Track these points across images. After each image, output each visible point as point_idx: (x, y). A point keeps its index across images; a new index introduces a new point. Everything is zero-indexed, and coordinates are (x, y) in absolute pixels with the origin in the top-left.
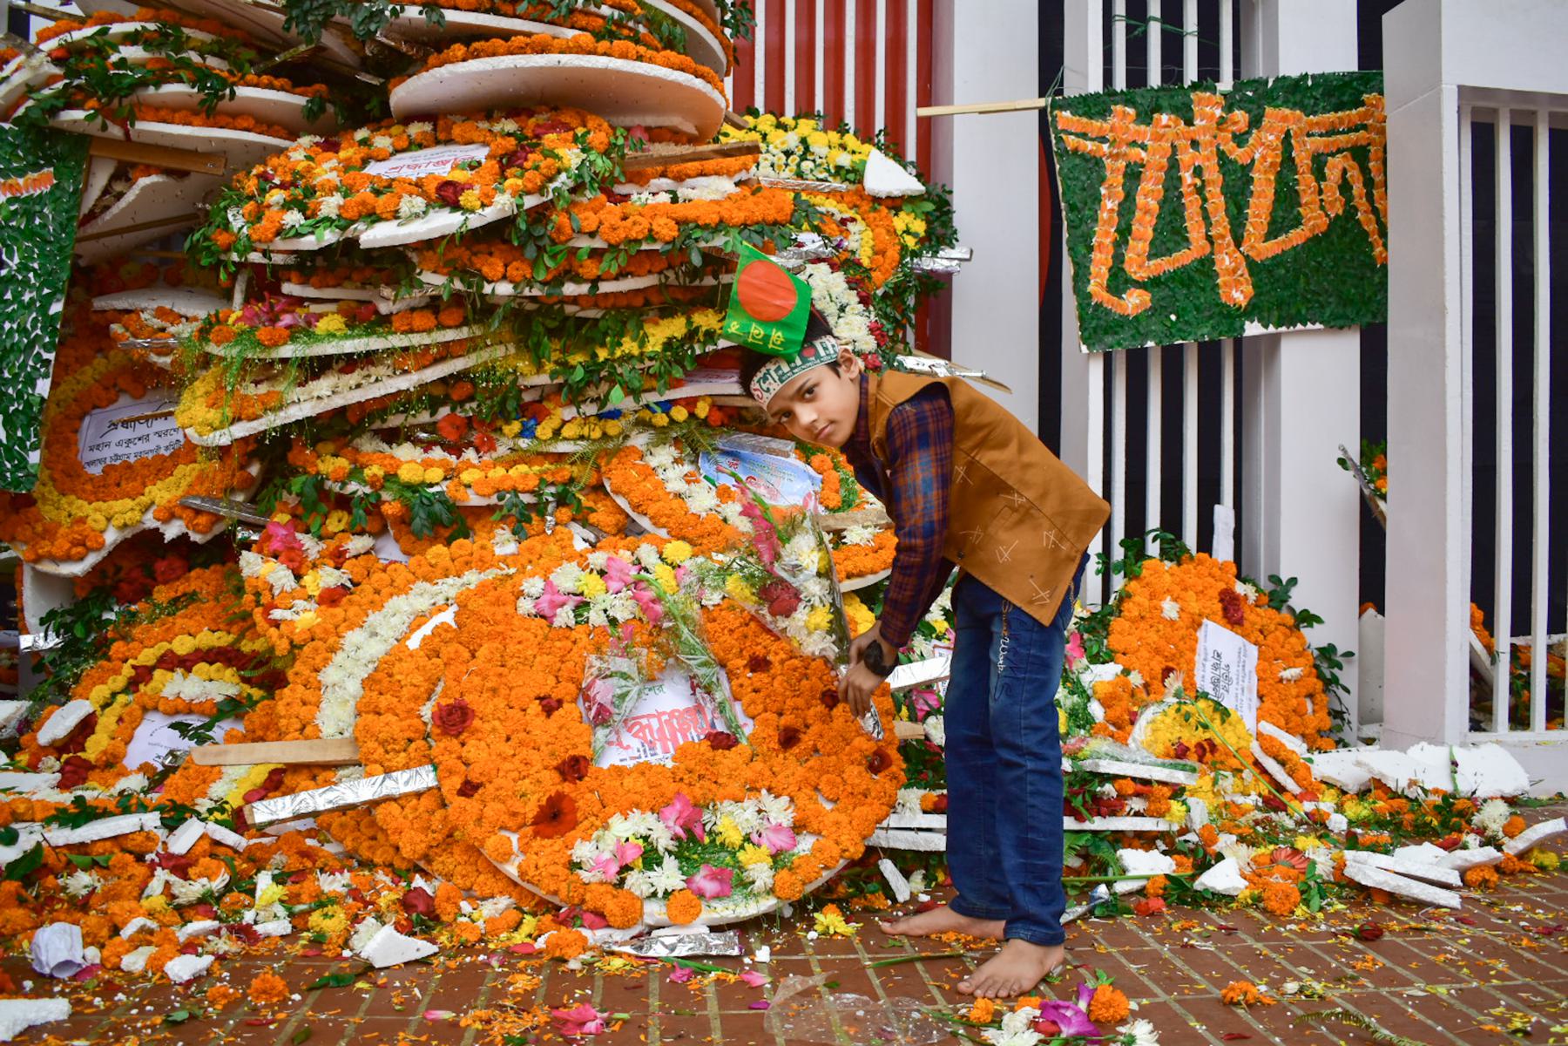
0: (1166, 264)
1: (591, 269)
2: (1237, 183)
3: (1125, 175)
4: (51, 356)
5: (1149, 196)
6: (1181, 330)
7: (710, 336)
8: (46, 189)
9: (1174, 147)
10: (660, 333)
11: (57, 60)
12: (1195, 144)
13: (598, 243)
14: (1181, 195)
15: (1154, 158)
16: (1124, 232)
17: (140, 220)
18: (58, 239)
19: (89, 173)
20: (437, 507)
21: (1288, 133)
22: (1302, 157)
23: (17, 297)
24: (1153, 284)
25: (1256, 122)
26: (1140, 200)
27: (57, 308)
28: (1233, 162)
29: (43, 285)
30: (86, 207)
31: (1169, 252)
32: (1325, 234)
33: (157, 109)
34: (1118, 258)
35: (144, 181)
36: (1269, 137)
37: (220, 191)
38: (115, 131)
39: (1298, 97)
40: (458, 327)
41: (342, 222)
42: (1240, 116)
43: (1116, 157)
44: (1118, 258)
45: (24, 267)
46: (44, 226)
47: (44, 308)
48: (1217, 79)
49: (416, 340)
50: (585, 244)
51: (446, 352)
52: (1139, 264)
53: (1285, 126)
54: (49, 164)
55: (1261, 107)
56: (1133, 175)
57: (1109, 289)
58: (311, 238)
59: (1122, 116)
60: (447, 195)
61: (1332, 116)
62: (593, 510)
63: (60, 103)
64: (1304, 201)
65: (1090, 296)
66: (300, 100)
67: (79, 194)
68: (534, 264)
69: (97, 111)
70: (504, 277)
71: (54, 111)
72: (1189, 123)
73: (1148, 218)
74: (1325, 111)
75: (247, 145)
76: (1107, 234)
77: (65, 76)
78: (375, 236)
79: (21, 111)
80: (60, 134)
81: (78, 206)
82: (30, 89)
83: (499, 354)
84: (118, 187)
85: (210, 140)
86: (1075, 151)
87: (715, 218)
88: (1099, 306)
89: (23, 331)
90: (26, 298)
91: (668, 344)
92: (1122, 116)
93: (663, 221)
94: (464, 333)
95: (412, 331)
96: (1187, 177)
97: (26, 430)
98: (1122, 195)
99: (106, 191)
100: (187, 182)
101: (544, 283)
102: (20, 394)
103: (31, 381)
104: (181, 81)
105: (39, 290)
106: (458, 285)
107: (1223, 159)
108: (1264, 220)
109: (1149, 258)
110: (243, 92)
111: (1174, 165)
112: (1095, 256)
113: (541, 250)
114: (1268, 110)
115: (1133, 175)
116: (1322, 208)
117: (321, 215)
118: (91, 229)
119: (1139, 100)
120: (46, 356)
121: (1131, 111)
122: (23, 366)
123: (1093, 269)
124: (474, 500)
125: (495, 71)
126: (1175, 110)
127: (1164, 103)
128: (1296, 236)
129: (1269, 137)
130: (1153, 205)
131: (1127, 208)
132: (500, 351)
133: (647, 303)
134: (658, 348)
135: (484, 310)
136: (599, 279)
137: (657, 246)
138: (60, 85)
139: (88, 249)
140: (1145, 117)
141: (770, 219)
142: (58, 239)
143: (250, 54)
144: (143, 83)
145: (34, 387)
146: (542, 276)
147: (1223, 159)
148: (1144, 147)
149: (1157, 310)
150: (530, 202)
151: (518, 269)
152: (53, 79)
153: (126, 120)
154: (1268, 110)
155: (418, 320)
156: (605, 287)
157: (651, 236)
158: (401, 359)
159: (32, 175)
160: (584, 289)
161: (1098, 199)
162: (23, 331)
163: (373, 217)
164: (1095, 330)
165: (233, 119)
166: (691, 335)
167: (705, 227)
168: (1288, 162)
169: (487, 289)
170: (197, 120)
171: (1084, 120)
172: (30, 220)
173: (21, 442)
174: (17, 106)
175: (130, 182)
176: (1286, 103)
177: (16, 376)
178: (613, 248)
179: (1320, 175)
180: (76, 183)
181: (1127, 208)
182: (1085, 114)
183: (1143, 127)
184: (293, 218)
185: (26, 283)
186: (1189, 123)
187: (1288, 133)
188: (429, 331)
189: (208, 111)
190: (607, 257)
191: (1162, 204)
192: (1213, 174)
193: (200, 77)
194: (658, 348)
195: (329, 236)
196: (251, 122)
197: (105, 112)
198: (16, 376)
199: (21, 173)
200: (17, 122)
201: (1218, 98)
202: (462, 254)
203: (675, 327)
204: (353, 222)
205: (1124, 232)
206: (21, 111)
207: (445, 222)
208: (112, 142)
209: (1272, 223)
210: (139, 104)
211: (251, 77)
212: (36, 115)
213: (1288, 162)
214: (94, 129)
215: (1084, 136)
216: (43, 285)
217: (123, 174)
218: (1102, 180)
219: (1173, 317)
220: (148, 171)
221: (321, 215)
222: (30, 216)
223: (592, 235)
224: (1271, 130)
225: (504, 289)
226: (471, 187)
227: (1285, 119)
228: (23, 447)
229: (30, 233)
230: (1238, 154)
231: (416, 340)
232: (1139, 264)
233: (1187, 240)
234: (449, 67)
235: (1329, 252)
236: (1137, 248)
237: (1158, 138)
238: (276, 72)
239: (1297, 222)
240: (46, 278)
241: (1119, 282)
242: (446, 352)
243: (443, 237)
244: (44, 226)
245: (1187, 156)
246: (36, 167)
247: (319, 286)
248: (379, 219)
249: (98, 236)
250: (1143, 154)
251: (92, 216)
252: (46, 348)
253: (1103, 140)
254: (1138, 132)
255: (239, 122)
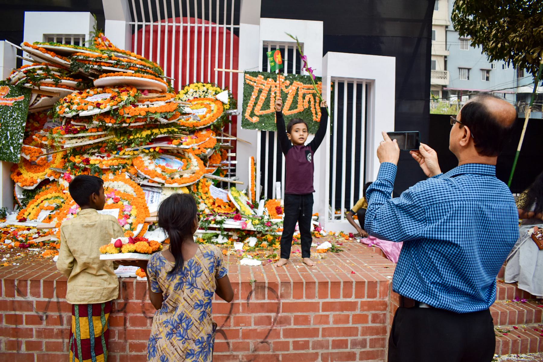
0: (264, 112)
1: (128, 121)
2: (284, 96)
3: (259, 91)
4: (23, 135)
5: (263, 97)
6: (266, 127)
7: (156, 134)
8: (23, 100)
9: (271, 87)
10: (145, 133)
11: (25, 73)
12: (276, 87)
13: (129, 116)
14: (270, 98)
15: (266, 88)
16: (256, 104)
17: (43, 106)
18: (25, 110)
19: (32, 96)
20: (96, 169)
21: (298, 88)
22: (301, 93)
23: (16, 122)
24: (260, 116)
25: (291, 84)
26: (261, 97)
27: (24, 125)
28: (284, 92)
29: (22, 120)
30: (31, 103)
31: (265, 110)
32: (302, 112)
33: (45, 84)
34: (253, 109)
35: (43, 98)
36: (293, 88)
37: (58, 102)
38: (37, 88)
39: (302, 80)
40: (102, 131)
41: (77, 111)
42: (288, 82)
43: (257, 87)
44: (253, 109)
45: (18, 116)
46: (22, 107)
47: (21, 125)
48: (284, 72)
49: (93, 134)
50: (126, 116)
51: (100, 136)
52: (258, 111)
53: (298, 86)
54: (23, 94)
55: (293, 81)
56: (260, 91)
57: (250, 116)
58: (70, 114)
59: (261, 77)
60: (98, 105)
61: (309, 85)
62: (129, 169)
63: (25, 82)
64: (299, 103)
65: (245, 117)
66: (76, 83)
67: (29, 101)
68: (116, 120)
69: (32, 84)
70: (110, 122)
71: (24, 84)
72: (275, 81)
73: (262, 101)
74: (308, 84)
75: (64, 91)
76: (252, 104)
77: (26, 77)
78: (82, 114)
79: (17, 83)
80: (25, 88)
81: (29, 103)
82: (19, 79)
83: (111, 137)
84: (38, 99)
85: (56, 90)
86: (248, 84)
87: (155, 111)
88: (247, 119)
89: (17, 129)
90: (18, 122)
91: (147, 135)
92: (261, 77)
93: (143, 111)
94: (103, 133)
95: (92, 132)
96: (273, 94)
97: (17, 150)
98: (257, 95)
99: (35, 100)
100: (53, 98)
101: (118, 124)
102: (16, 142)
103: (19, 140)
104: (49, 78)
105: (21, 121)
106: (101, 124)
107: (282, 91)
108: (288, 107)
109: (261, 110)
110: (63, 81)
111: (270, 91)
112: (248, 108)
113: (117, 117)
114: (295, 82)
115: (260, 91)
116: (303, 106)
117: (73, 109)
118: (33, 107)
119: (265, 75)
120: (22, 135)
121: (263, 77)
122: (17, 136)
123: (247, 110)
124: (104, 167)
125: (116, 79)
126: (273, 78)
127: (271, 76)
128: (295, 111)
129: (293, 88)
130: (264, 98)
131: (257, 98)
132: (112, 136)
133: (144, 127)
134: (144, 136)
135: (106, 128)
136: (131, 123)
137: (141, 117)
138: (25, 79)
139: (32, 111)
140: (266, 78)
141: (168, 111)
142: (25, 110)
143: (66, 72)
144: (42, 79)
145: (19, 141)
146: (118, 122)
147: (282, 91)
148: (264, 85)
149: (260, 122)
150: (114, 107)
151: (113, 121)
152: (24, 77)
153: (39, 86)
154: (295, 82)
155: (93, 130)
156: (132, 125)
157: (140, 115)
158: (90, 137)
159: (19, 97)
160: (127, 125)
161: (251, 95)
162: (17, 129)
163: (83, 110)
164: (245, 124)
165: (61, 86)
166: (152, 134)
167: (152, 113)
168: (297, 94)
169: (107, 125)
170: (53, 86)
171: (252, 77)
172: (19, 106)
173: (16, 152)
174: (17, 82)
175: (40, 98)
176: (299, 81)
177: (16, 139)
178: (132, 117)
179: (304, 98)
180: (29, 98)
181: (257, 98)
182: (252, 76)
183: (265, 81)
184: (67, 110)
185: (18, 119)
186: (275, 81)
187: (298, 88)
188: (96, 132)
189: (57, 84)
190: (131, 119)
191: (266, 99)
192: (278, 94)
193: (53, 76)
194: (144, 136)
195: (74, 113)
196: (65, 87)
197: (34, 84)
198: (16, 139)
199: (17, 96)
200: (16, 86)
201: (284, 77)
202: (102, 117)
203: (149, 132)
204: (79, 111)
205: (256, 104)
206: (17, 83)
207: (97, 111)
208: (36, 90)
209: (291, 107)
210: (41, 83)
211: (65, 78)
212: (20, 85)
213: (297, 94)
214: (32, 87)
215: (251, 81)
216: (22, 120)
217: (39, 96)
218: (253, 91)
219: (263, 124)
220: (44, 96)
221: (73, 109)
222: (19, 105)
223: (128, 114)
224: (294, 86)
225: (110, 125)
226: (103, 104)
227: (298, 84)
228: (17, 154)
229: (19, 109)
230: (285, 91)
231: (93, 134)
232: (258, 111)
233: (270, 108)
234: (103, 78)
235: (302, 116)
236: (258, 108)
237: (267, 84)
238: (71, 76)
239: (296, 108)
240: (22, 118)
241: (252, 114)
242: (100, 136)
243: (96, 115)
244: (22, 107)
245: (273, 89)
246: (21, 95)
247: (77, 122)
248: (84, 110)
249: (34, 109)
250: (264, 87)
251: (32, 105)
252: (22, 133)
253: (255, 82)
254: (263, 82)
255: (63, 87)
